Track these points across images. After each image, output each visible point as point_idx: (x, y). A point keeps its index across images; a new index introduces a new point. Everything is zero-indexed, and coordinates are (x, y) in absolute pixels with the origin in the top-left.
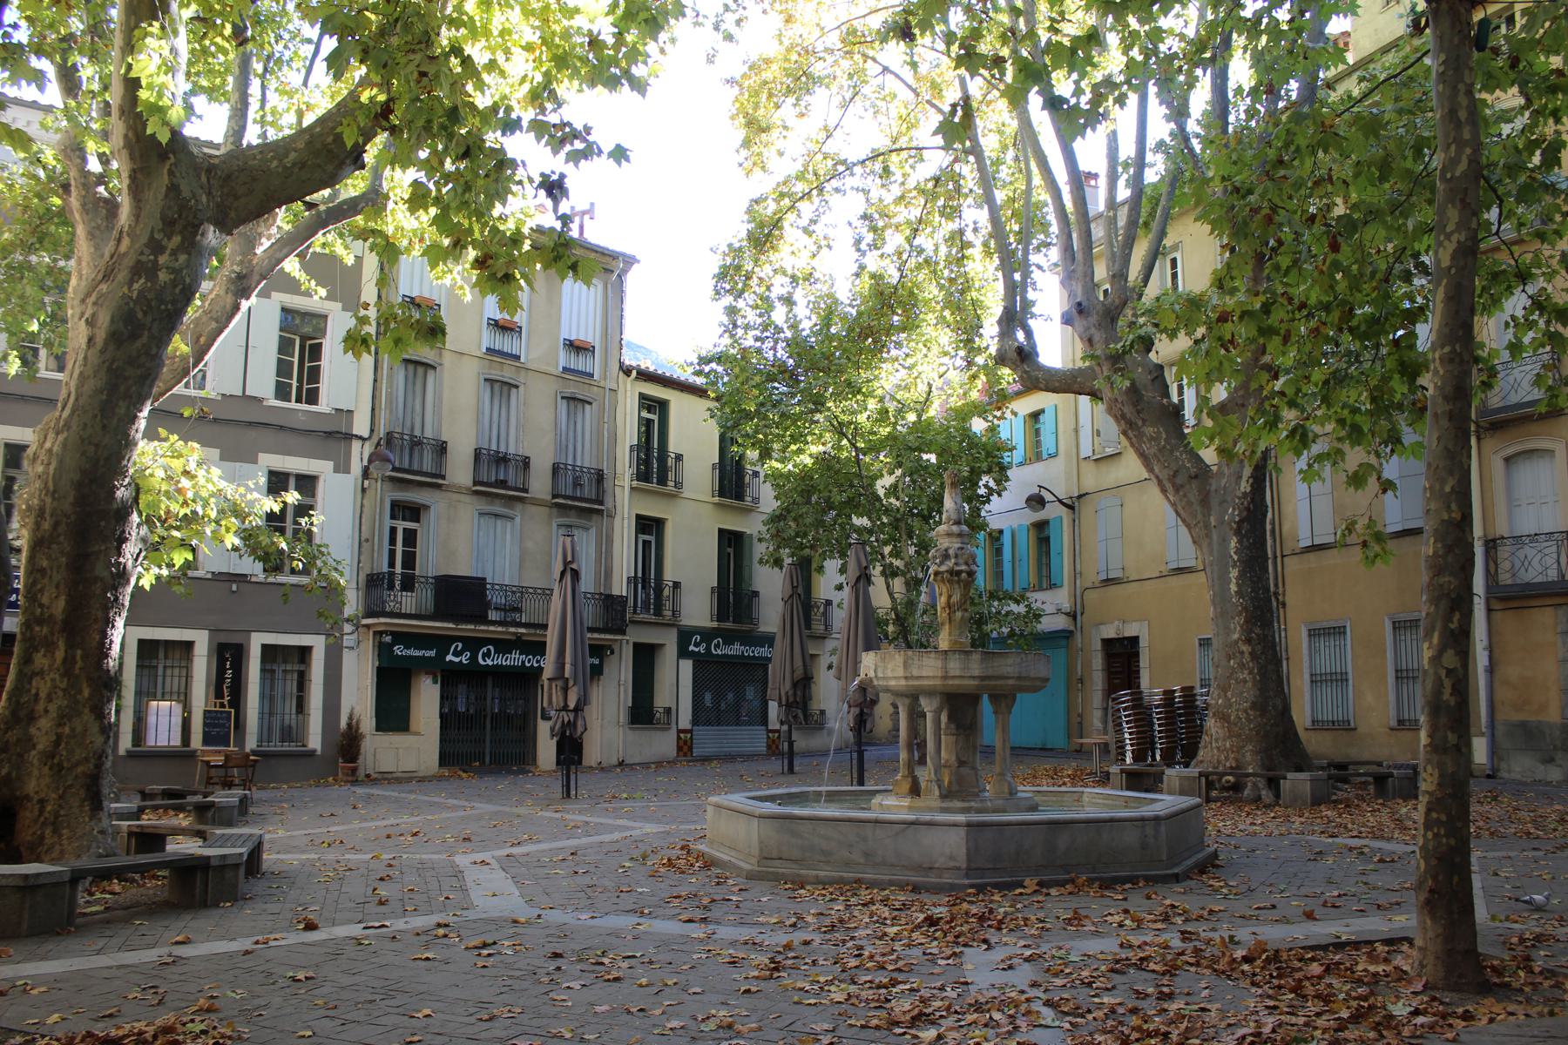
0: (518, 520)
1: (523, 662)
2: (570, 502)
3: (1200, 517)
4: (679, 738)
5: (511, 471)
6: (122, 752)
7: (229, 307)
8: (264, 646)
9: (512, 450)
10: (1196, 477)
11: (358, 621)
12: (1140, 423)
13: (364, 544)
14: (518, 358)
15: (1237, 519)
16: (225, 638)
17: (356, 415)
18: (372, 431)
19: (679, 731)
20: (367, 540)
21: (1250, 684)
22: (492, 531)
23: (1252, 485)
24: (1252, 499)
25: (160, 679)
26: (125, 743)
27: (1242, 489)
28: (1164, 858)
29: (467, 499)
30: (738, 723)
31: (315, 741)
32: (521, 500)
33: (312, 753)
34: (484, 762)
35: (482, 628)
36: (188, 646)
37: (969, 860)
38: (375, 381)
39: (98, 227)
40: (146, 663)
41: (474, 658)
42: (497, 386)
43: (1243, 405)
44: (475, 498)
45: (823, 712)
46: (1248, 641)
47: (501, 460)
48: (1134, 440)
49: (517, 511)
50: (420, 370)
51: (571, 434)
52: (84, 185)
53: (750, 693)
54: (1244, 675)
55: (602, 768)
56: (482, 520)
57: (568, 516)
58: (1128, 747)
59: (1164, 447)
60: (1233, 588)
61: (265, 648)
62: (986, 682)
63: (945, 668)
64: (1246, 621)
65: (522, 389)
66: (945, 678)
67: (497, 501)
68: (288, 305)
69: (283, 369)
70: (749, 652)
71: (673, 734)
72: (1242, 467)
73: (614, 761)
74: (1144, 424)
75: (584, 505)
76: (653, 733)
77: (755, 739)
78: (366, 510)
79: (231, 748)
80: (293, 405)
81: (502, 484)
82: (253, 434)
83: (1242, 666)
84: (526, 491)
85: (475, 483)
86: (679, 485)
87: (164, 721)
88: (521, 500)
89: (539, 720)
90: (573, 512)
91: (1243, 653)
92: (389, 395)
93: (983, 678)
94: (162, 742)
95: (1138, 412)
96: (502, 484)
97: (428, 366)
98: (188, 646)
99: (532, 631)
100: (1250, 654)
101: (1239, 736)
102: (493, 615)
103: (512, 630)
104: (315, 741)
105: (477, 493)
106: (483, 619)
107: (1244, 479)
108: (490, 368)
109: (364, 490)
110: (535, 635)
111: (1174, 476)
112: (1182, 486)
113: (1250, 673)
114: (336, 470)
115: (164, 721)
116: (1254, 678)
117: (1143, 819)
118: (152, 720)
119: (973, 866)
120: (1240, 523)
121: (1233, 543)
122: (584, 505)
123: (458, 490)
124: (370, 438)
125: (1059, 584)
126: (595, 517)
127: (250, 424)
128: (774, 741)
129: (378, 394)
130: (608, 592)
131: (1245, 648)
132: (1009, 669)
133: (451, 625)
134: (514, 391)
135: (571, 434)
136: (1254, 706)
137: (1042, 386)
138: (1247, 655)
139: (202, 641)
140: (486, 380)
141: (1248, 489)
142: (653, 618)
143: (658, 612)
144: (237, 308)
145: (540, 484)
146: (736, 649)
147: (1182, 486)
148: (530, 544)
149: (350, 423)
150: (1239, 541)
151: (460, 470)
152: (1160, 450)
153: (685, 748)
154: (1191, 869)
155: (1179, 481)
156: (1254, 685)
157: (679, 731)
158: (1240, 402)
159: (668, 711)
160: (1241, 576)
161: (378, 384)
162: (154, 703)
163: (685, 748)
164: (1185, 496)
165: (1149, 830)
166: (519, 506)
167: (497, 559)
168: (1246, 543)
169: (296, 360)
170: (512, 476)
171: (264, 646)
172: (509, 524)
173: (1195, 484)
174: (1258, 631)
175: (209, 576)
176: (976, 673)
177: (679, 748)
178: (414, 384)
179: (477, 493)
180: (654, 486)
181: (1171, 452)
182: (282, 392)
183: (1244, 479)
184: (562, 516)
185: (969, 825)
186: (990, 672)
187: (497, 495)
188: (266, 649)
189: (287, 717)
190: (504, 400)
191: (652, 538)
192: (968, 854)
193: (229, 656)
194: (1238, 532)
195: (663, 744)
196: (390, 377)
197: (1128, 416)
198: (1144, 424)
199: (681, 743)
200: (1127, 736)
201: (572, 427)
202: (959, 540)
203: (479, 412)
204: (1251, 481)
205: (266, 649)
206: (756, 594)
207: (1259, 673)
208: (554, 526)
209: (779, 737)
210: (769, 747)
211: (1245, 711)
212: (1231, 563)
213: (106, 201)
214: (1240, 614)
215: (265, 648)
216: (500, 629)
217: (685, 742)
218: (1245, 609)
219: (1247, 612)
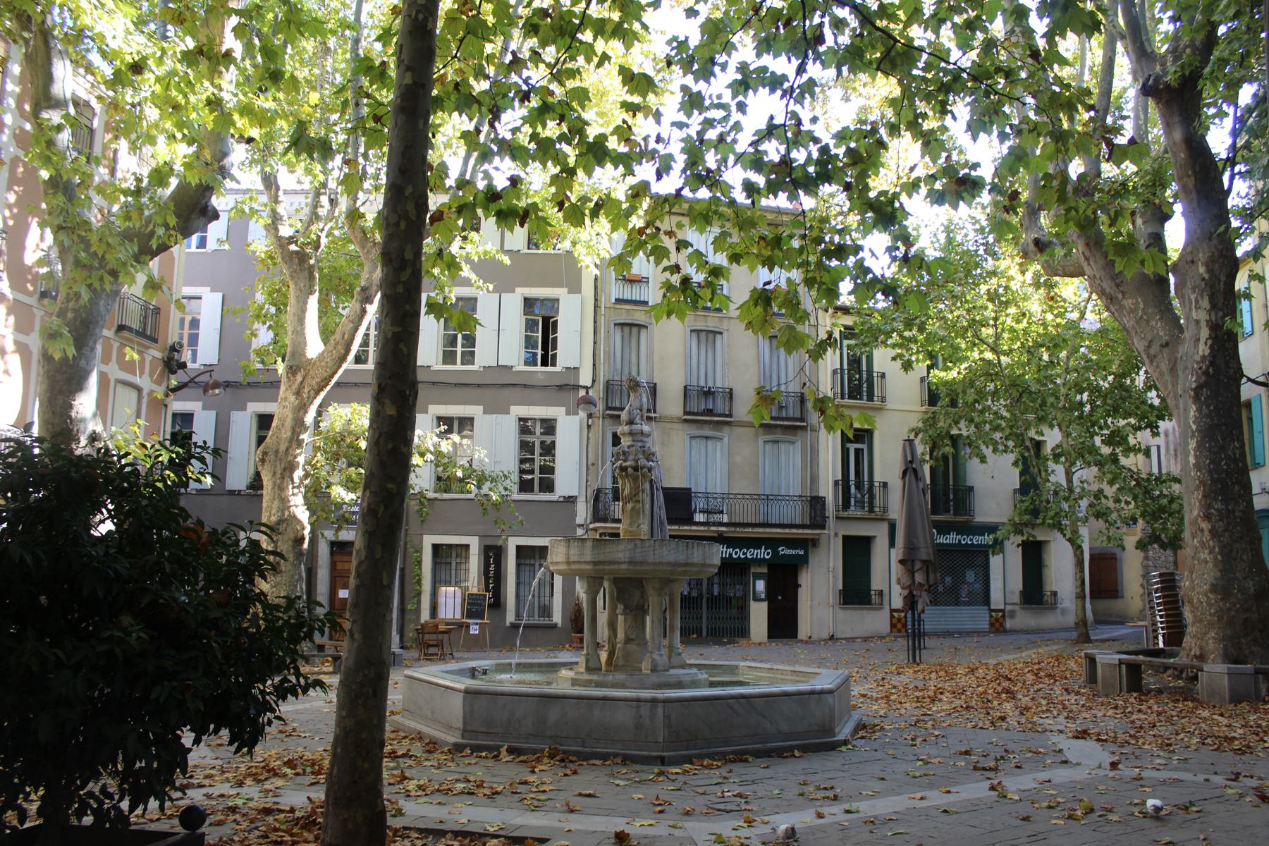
0: (726, 440)
1: (731, 555)
2: (778, 423)
3: (1170, 387)
4: (892, 617)
5: (719, 402)
6: (508, 624)
7: (358, 311)
8: (518, 547)
9: (719, 384)
10: (1167, 344)
11: (588, 526)
12: (1120, 296)
13: (591, 467)
14: (646, 303)
15: (1194, 385)
16: (489, 542)
17: (581, 371)
18: (594, 381)
19: (892, 611)
20: (593, 464)
21: (1210, 565)
22: (703, 451)
23: (1211, 347)
24: (1212, 363)
25: (453, 572)
26: (425, 616)
27: (1201, 353)
28: (661, 740)
29: (679, 426)
30: (957, 603)
31: (557, 618)
32: (728, 423)
33: (555, 626)
34: (701, 635)
35: (686, 528)
36: (467, 547)
37: (465, 723)
38: (595, 343)
39: (295, 271)
40: (522, 562)
41: (775, 552)
42: (703, 335)
43: (1193, 262)
44: (686, 425)
45: (1055, 594)
46: (1207, 517)
47: (708, 393)
48: (1116, 314)
49: (725, 433)
50: (635, 330)
51: (775, 367)
52: (280, 246)
53: (970, 576)
54: (1205, 555)
55: (809, 641)
56: (694, 442)
57: (774, 434)
58: (1160, 631)
59: (1141, 318)
60: (1192, 460)
61: (519, 548)
62: (601, 567)
63: (568, 555)
64: (1204, 496)
65: (725, 334)
66: (568, 563)
67: (706, 426)
68: (528, 296)
69: (529, 342)
70: (966, 540)
71: (885, 613)
72: (1199, 328)
73: (826, 636)
74: (1124, 297)
75: (786, 423)
76: (865, 612)
77: (978, 618)
78: (591, 441)
79: (485, 621)
80: (539, 368)
81: (710, 412)
82: (506, 392)
83: (1203, 544)
84: (730, 415)
85: (686, 413)
86: (883, 399)
87: (450, 601)
88: (728, 423)
89: (752, 602)
90: (778, 430)
91: (1202, 530)
92: (607, 353)
93: (595, 563)
94: (450, 616)
95: (1118, 286)
96: (710, 412)
97: (640, 326)
98: (467, 547)
99: (732, 529)
100: (1210, 531)
101: (1201, 621)
102: (699, 517)
103: (713, 528)
104: (557, 618)
105: (686, 421)
106: (690, 521)
107: (1202, 341)
108: (695, 321)
109: (589, 426)
110: (735, 532)
111: (1149, 347)
112: (1155, 356)
113: (1210, 553)
114: (568, 413)
115: (450, 601)
116: (1215, 558)
117: (638, 700)
118: (441, 600)
119: (468, 728)
120: (1197, 390)
121: (1192, 411)
122: (786, 423)
123: (671, 420)
124: (592, 386)
125: (1262, 464)
126: (800, 433)
127: (503, 385)
128: (997, 620)
129: (597, 352)
130: (815, 494)
131: (1205, 525)
132: (621, 555)
133: (677, 527)
134: (718, 337)
135: (775, 367)
136: (1214, 589)
137: (1060, 272)
138: (1206, 533)
139: (474, 543)
140: (692, 331)
141: (1207, 352)
142: (867, 515)
143: (871, 510)
144: (364, 312)
145: (744, 407)
146: (953, 538)
147: (1155, 356)
148: (738, 459)
149: (577, 376)
150: (1199, 410)
151: (671, 404)
152: (1137, 322)
153: (899, 626)
154: (717, 754)
155: (1152, 352)
156: (1216, 566)
157: (892, 611)
158: (1189, 259)
159: (881, 593)
160: (1200, 445)
161: (597, 345)
162: (444, 588)
163: (899, 626)
164: (1157, 366)
165: (645, 710)
166: (727, 429)
167: (709, 473)
168: (1205, 410)
169: (540, 335)
170: (720, 406)
171: (518, 547)
172: (719, 444)
173: (1166, 351)
174: (1219, 506)
175: (562, 499)
176: (588, 558)
177: (893, 626)
178: (630, 341)
179: (686, 421)
180: (864, 402)
181: (1148, 321)
182: (531, 361)
183: (1202, 341)
184: (767, 434)
185: (467, 692)
186: (602, 558)
187: (706, 422)
188: (519, 549)
189: (542, 599)
190: (710, 345)
191: (864, 446)
192: (464, 717)
193: (493, 554)
194: (1197, 398)
195: (877, 621)
196: (607, 338)
197: (1108, 290)
198: (1124, 297)
199: (895, 621)
200: (1158, 618)
201: (775, 360)
202: (630, 438)
203: (759, 358)
204: (1210, 342)
205: (519, 549)
206: (971, 489)
207: (1221, 552)
208: (761, 442)
209: (1003, 616)
210: (992, 625)
211: (1206, 594)
212: (1190, 434)
213: (297, 253)
214: (1198, 488)
215: (519, 548)
216: (702, 528)
217: (899, 620)
218: (1202, 483)
219: (1204, 486)
